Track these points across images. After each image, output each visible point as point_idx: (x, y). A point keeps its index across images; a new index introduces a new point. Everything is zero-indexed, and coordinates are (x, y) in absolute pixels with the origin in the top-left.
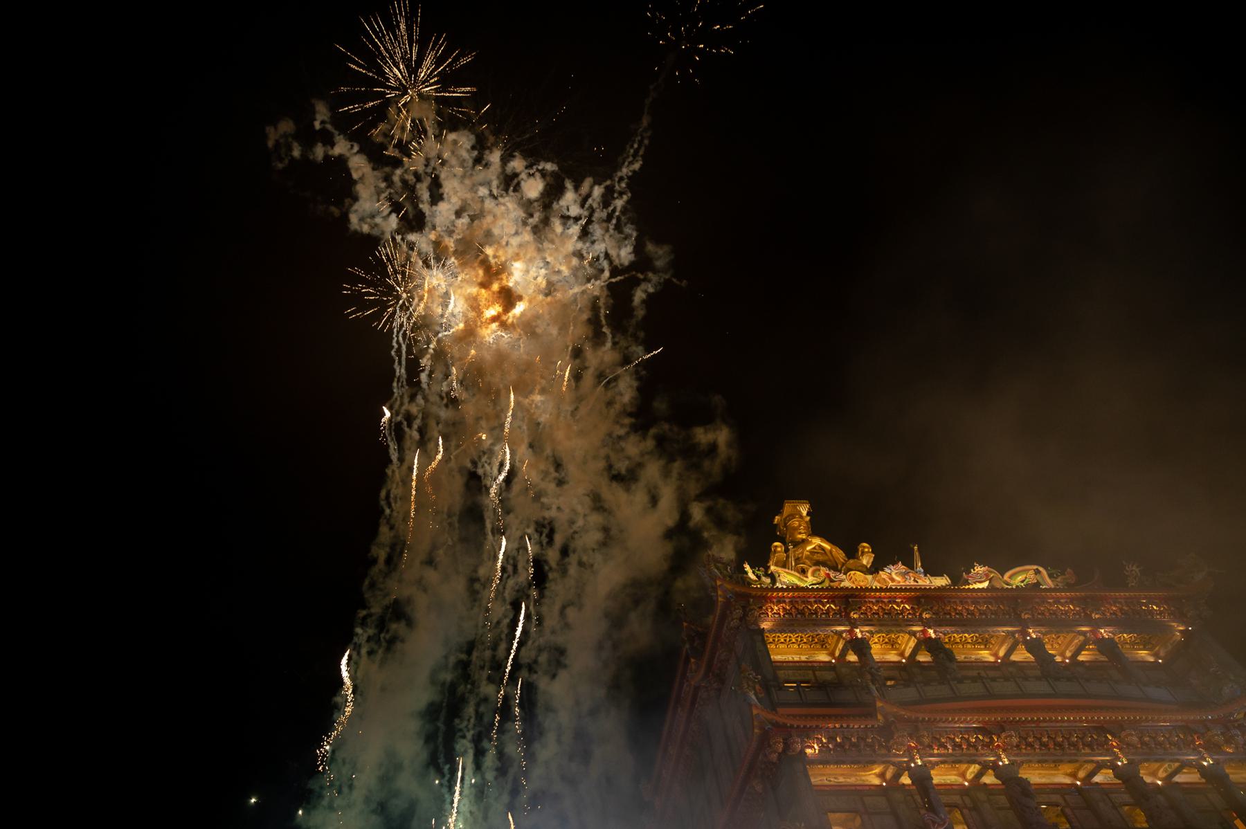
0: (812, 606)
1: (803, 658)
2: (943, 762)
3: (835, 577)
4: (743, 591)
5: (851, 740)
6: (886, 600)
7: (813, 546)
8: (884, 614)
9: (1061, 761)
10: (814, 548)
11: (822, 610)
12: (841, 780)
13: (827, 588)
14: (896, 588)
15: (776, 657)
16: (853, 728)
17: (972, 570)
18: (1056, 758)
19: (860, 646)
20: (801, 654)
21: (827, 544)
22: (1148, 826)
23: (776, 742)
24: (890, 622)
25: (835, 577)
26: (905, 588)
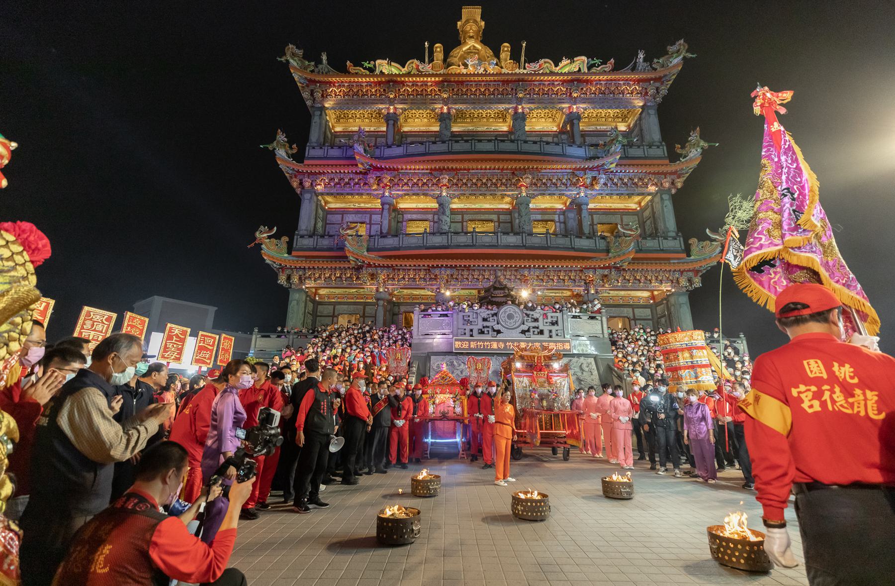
0: (621, 87)
1: (372, 129)
2: (406, 195)
3: (423, 68)
4: (644, 76)
5: (613, 180)
6: (419, 84)
7: (468, 47)
8: (435, 95)
9: (633, 194)
10: (469, 49)
11: (628, 90)
12: (362, 205)
13: (497, 74)
14: (425, 74)
15: (406, 129)
16: (629, 172)
17: (439, 54)
18: (482, 192)
19: (392, 120)
20: (371, 126)
21: (479, 45)
22: (262, 235)
23: (307, 181)
24: (420, 99)
25: (423, 68)
26: (425, 74)
